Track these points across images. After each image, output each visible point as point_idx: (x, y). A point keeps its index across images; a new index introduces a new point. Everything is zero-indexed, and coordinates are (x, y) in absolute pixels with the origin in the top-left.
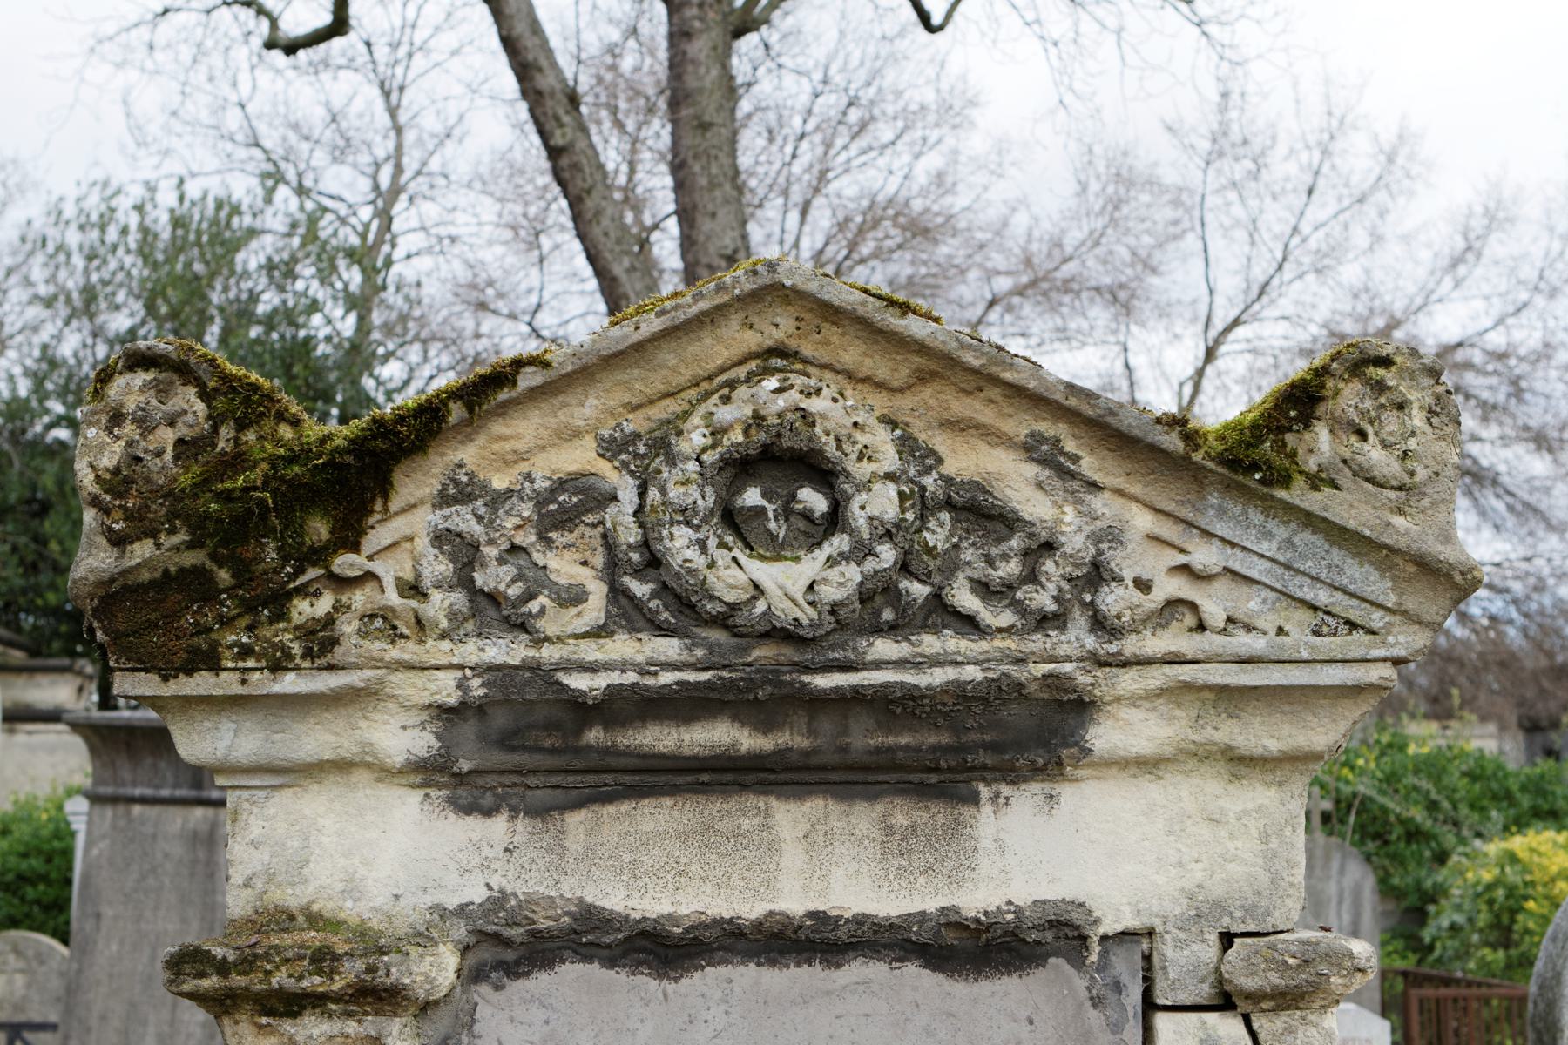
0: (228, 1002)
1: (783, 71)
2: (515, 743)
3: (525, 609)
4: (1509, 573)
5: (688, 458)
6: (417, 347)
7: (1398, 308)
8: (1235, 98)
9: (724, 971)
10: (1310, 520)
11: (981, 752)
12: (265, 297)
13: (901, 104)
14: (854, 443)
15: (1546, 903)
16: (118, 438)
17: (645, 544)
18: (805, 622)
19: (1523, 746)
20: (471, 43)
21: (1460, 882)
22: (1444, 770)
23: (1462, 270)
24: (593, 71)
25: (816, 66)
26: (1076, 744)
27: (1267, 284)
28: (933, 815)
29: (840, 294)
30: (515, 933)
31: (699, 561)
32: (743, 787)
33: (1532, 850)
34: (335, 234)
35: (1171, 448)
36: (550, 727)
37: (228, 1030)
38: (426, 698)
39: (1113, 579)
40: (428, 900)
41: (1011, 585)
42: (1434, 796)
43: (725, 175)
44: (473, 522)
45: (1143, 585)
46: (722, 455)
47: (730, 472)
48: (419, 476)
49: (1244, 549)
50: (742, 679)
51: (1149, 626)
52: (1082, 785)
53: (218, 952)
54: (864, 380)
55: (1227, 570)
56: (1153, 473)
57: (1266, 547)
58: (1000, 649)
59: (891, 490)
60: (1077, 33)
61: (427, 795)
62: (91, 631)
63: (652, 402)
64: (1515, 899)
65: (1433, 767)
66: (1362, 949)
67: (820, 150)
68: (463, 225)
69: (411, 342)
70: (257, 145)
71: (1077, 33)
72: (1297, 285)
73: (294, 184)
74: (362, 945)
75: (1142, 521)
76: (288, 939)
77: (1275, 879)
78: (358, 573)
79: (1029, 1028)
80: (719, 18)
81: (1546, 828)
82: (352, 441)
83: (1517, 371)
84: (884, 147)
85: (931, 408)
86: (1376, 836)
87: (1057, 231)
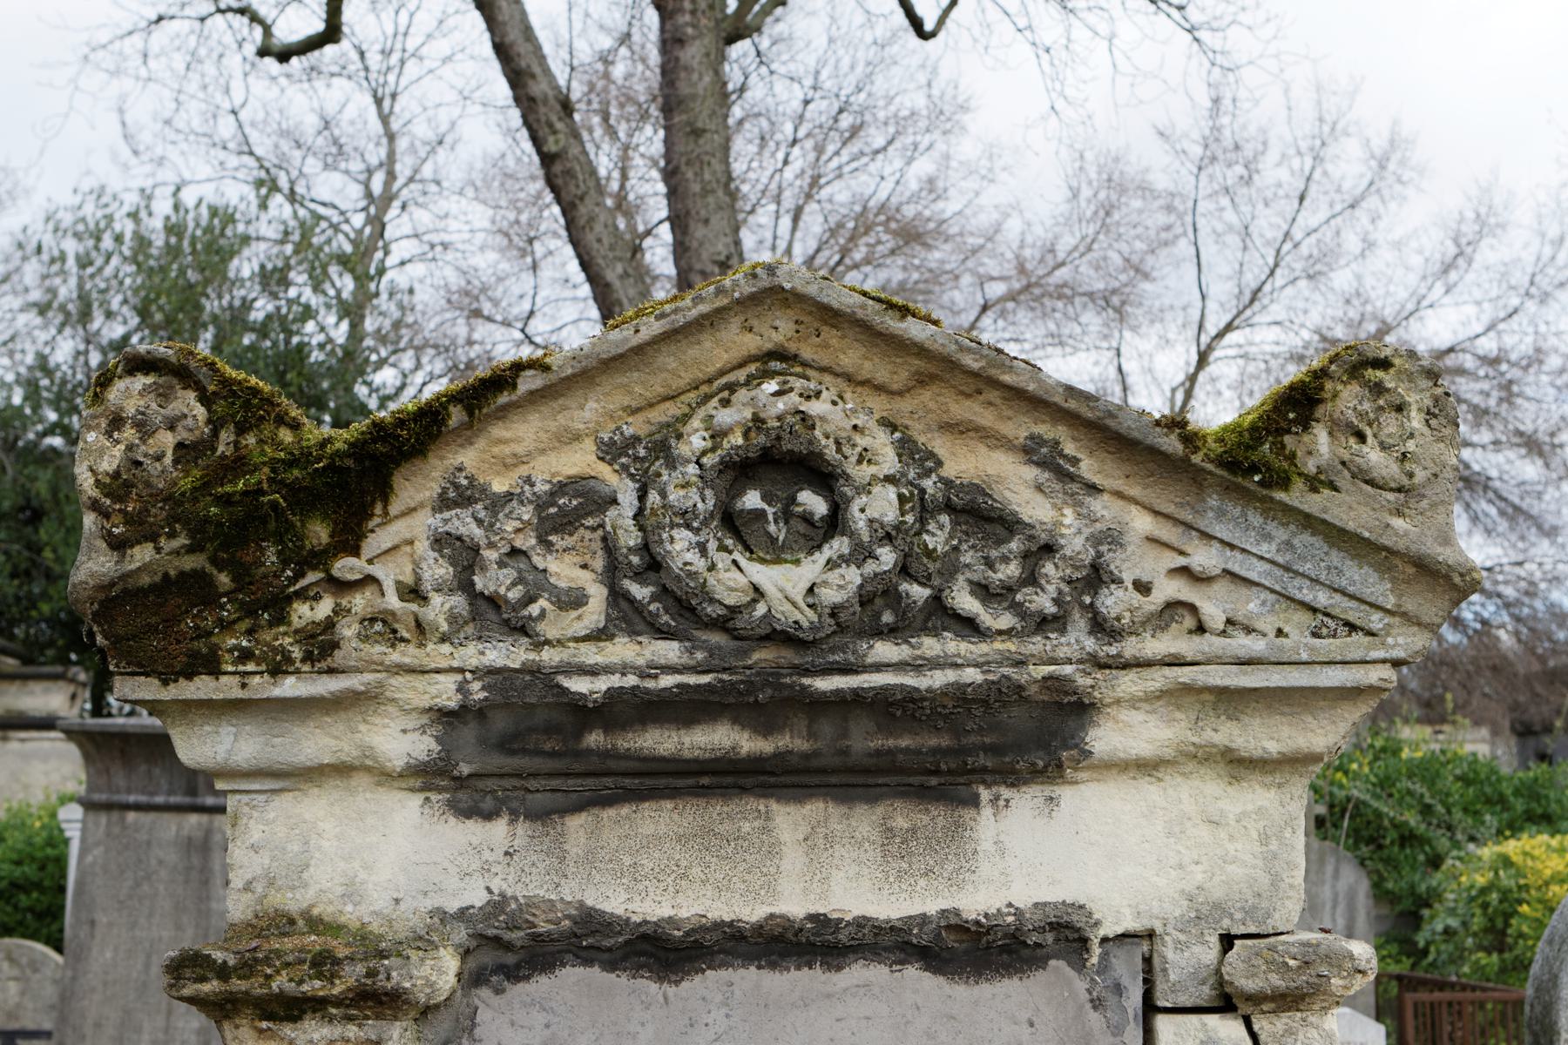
0: (229, 1006)
1: (775, 77)
2: (516, 746)
3: (525, 613)
4: (1500, 578)
5: (688, 461)
6: (411, 353)
7: (1389, 313)
8: (1227, 103)
9: (724, 974)
10: (1309, 522)
11: (982, 755)
12: (258, 304)
13: (892, 108)
14: (854, 445)
15: (1540, 906)
16: (118, 442)
17: (645, 548)
18: (805, 624)
19: (1515, 750)
20: (462, 50)
21: (1454, 886)
22: (1438, 774)
23: (1453, 276)
24: (586, 77)
25: (807, 72)
26: (1076, 746)
27: (1259, 289)
28: (934, 818)
29: (839, 297)
30: (516, 936)
31: (699, 564)
32: (743, 790)
33: (1526, 854)
34: (329, 241)
35: (1170, 450)
36: (550, 730)
37: (228, 1035)
38: (426, 702)
39: (1113, 582)
41: (1009, 589)
42: (1428, 800)
43: (718, 181)
44: (473, 526)
45: (1143, 588)
46: (722, 458)
47: (730, 475)
48: (419, 479)
49: (1244, 550)
50: (742, 682)
51: (1149, 628)
52: (1082, 787)
53: (218, 956)
54: (863, 383)
55: (1227, 572)
56: (1152, 475)
57: (1266, 549)
58: (1000, 652)
59: (891, 493)
60: (1069, 40)
61: (427, 799)
62: (91, 635)
63: (651, 405)
64: (1511, 901)
65: (1428, 770)
66: (1362, 950)
67: (812, 156)
68: (455, 232)
69: (404, 350)
70: (251, 153)
71: (1069, 40)
72: (1289, 291)
73: (286, 190)
74: (362, 949)
75: (1142, 523)
76: (288, 943)
77: (1276, 881)
78: (358, 576)
79: (1030, 1030)
80: (712, 24)
81: (1539, 832)
82: (352, 445)
83: (1508, 376)
84: (877, 152)
85: (930, 411)
86: (1371, 840)
87: (1050, 235)
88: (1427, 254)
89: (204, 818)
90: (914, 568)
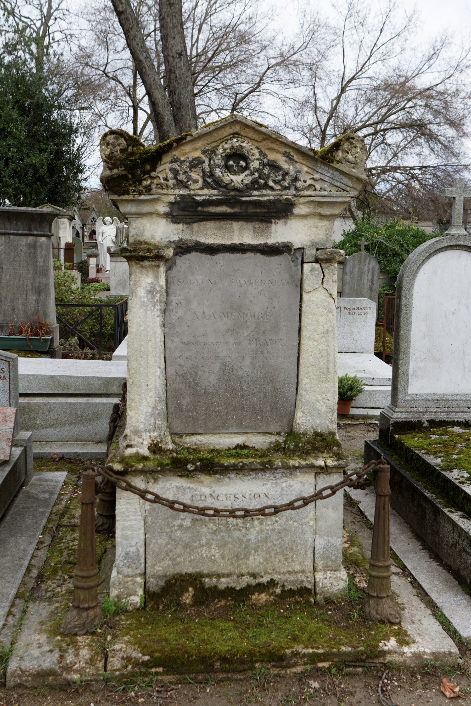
9: (223, 254)
17: (210, 172)
23: (432, 62)
28: (264, 225)
30: (184, 246)
31: (221, 175)
38: (168, 201)
40: (167, 240)
53: (129, 248)
55: (321, 179)
57: (328, 175)
59: (258, 162)
75: (305, 169)
76: (142, 246)
88: (424, 53)
89: (34, 238)
90: (262, 177)
